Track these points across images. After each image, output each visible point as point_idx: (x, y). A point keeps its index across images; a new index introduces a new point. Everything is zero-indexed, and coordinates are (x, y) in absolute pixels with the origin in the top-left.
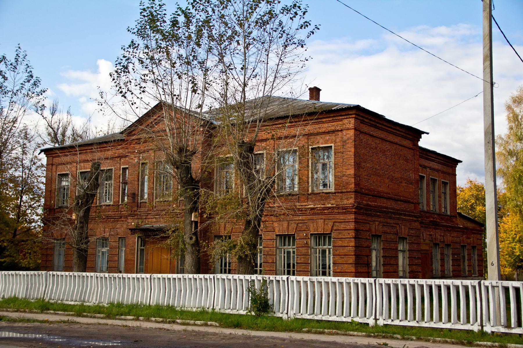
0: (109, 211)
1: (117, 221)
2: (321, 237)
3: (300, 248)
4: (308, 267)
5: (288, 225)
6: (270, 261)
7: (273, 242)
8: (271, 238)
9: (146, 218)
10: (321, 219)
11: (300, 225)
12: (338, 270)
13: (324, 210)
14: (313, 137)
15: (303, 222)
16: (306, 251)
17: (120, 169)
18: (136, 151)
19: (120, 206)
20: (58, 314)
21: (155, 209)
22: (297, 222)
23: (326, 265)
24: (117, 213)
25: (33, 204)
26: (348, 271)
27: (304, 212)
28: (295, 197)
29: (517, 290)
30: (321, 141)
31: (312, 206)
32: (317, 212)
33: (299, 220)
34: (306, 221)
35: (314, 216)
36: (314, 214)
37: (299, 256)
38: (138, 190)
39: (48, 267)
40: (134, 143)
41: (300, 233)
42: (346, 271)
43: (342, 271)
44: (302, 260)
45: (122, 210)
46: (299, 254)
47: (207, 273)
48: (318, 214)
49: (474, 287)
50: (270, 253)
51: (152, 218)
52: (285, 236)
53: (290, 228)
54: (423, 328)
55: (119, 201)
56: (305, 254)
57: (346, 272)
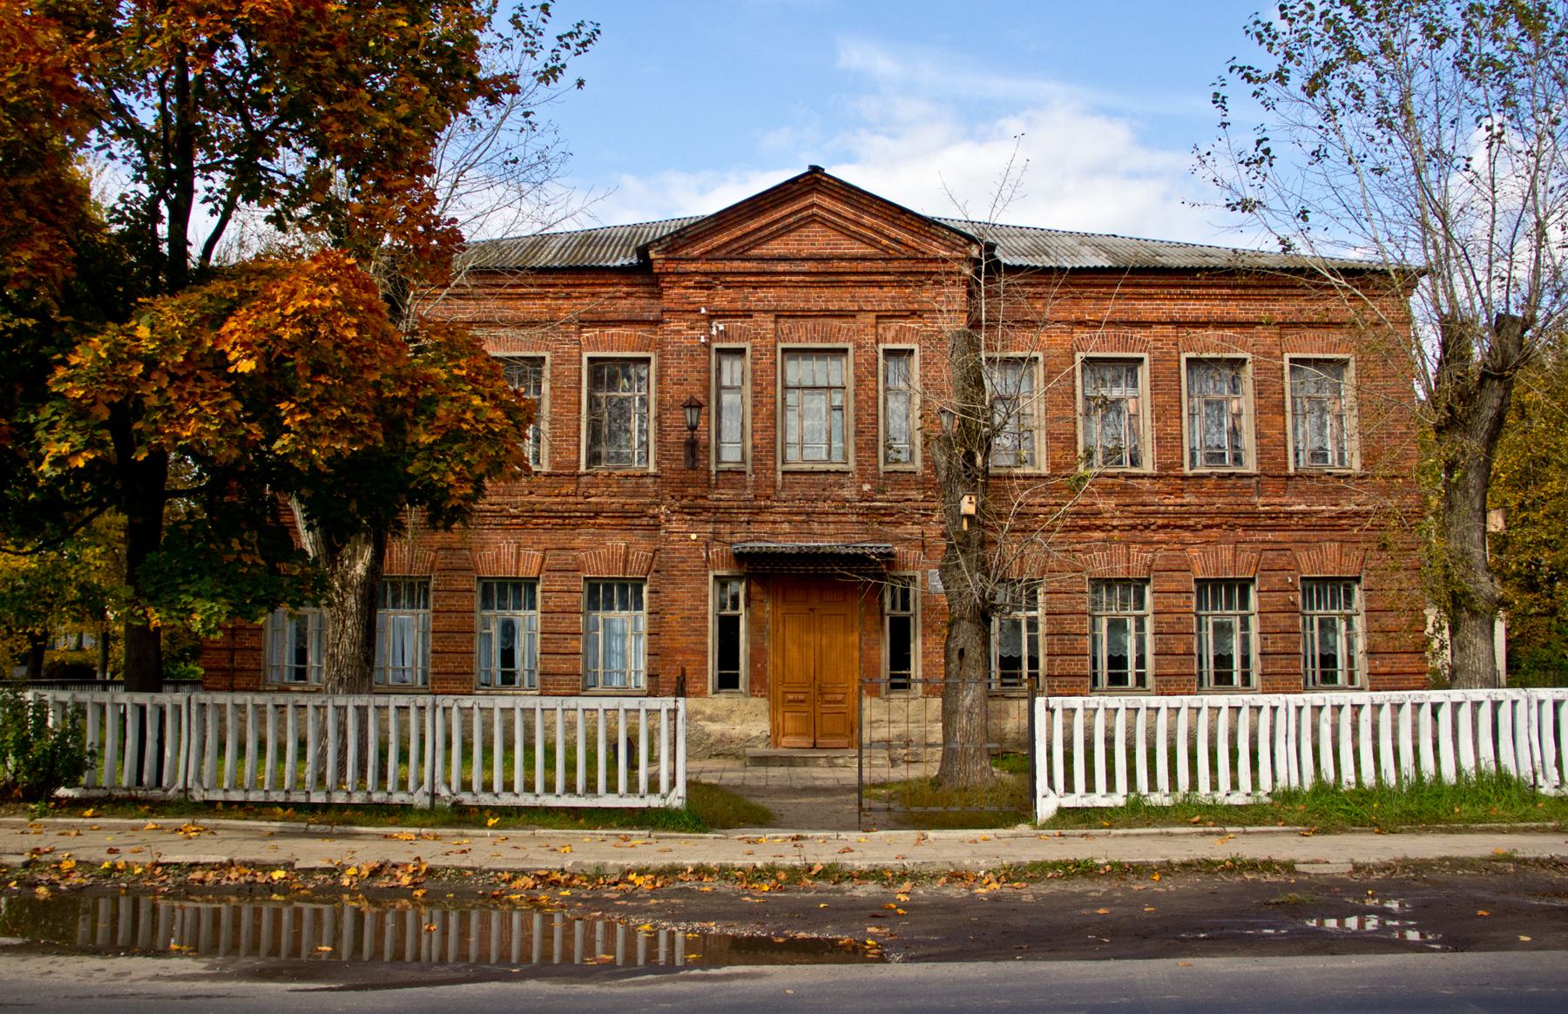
0: (531, 493)
1: (577, 526)
2: (1233, 589)
3: (1270, 615)
4: (1297, 663)
5: (1235, 555)
6: (1181, 649)
7: (1188, 598)
8: (1182, 589)
9: (748, 523)
10: (1332, 540)
11: (1270, 555)
12: (1382, 670)
13: (1340, 518)
14: (1294, 331)
15: (1275, 546)
16: (1289, 622)
17: (580, 361)
18: (703, 311)
19: (584, 480)
20: (358, 834)
21: (783, 495)
22: (1261, 546)
23: (1230, 657)
24: (571, 499)
25: (75, 453)
26: (1410, 670)
27: (1282, 522)
28: (1246, 481)
29: (1557, 705)
30: (1319, 343)
31: (1303, 507)
32: (1319, 523)
33: (1264, 542)
34: (1287, 546)
35: (1311, 533)
36: (1308, 528)
37: (1269, 636)
38: (709, 431)
39: (243, 670)
40: (692, 284)
41: (1270, 576)
42: (1406, 669)
43: (1394, 670)
44: (1280, 646)
45: (593, 491)
46: (1270, 629)
47: (257, 691)
48: (1322, 528)
49: (178, 708)
50: (1178, 627)
51: (774, 522)
52: (1216, 583)
53: (1239, 563)
54: (1026, 798)
55: (578, 461)
56: (1283, 629)
57: (1404, 673)
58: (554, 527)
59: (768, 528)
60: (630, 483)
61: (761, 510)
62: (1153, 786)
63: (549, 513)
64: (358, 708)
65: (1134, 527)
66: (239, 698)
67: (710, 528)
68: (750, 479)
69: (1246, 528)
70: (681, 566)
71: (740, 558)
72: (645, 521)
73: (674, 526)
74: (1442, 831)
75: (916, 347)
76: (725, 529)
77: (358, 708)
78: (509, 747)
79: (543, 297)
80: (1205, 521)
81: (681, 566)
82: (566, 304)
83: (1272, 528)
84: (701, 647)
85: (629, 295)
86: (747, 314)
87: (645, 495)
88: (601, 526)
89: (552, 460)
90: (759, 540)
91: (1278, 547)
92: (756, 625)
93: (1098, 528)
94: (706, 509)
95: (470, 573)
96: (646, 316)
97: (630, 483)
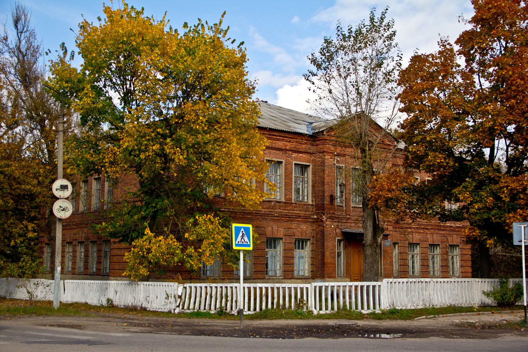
1: (293, 221)
58: (287, 221)
59: (349, 224)
60: (305, 207)
61: (349, 219)
62: (362, 308)
63: (286, 216)
64: (248, 287)
65: (417, 228)
66: (226, 285)
67: (336, 224)
68: (344, 208)
69: (438, 230)
70: (330, 236)
71: (344, 234)
72: (311, 220)
73: (328, 223)
74: (271, 328)
75: (283, 161)
76: (340, 224)
77: (248, 287)
78: (326, 299)
79: (283, 140)
80: (431, 227)
81: (330, 236)
82: (289, 144)
83: (443, 230)
84: (334, 262)
85: (306, 143)
86: (344, 155)
87: (308, 211)
88: (299, 221)
89: (285, 197)
90: (347, 228)
91: (444, 236)
92: (347, 257)
93: (410, 228)
94: (336, 218)
95: (264, 236)
96: (309, 151)
97: (305, 207)
